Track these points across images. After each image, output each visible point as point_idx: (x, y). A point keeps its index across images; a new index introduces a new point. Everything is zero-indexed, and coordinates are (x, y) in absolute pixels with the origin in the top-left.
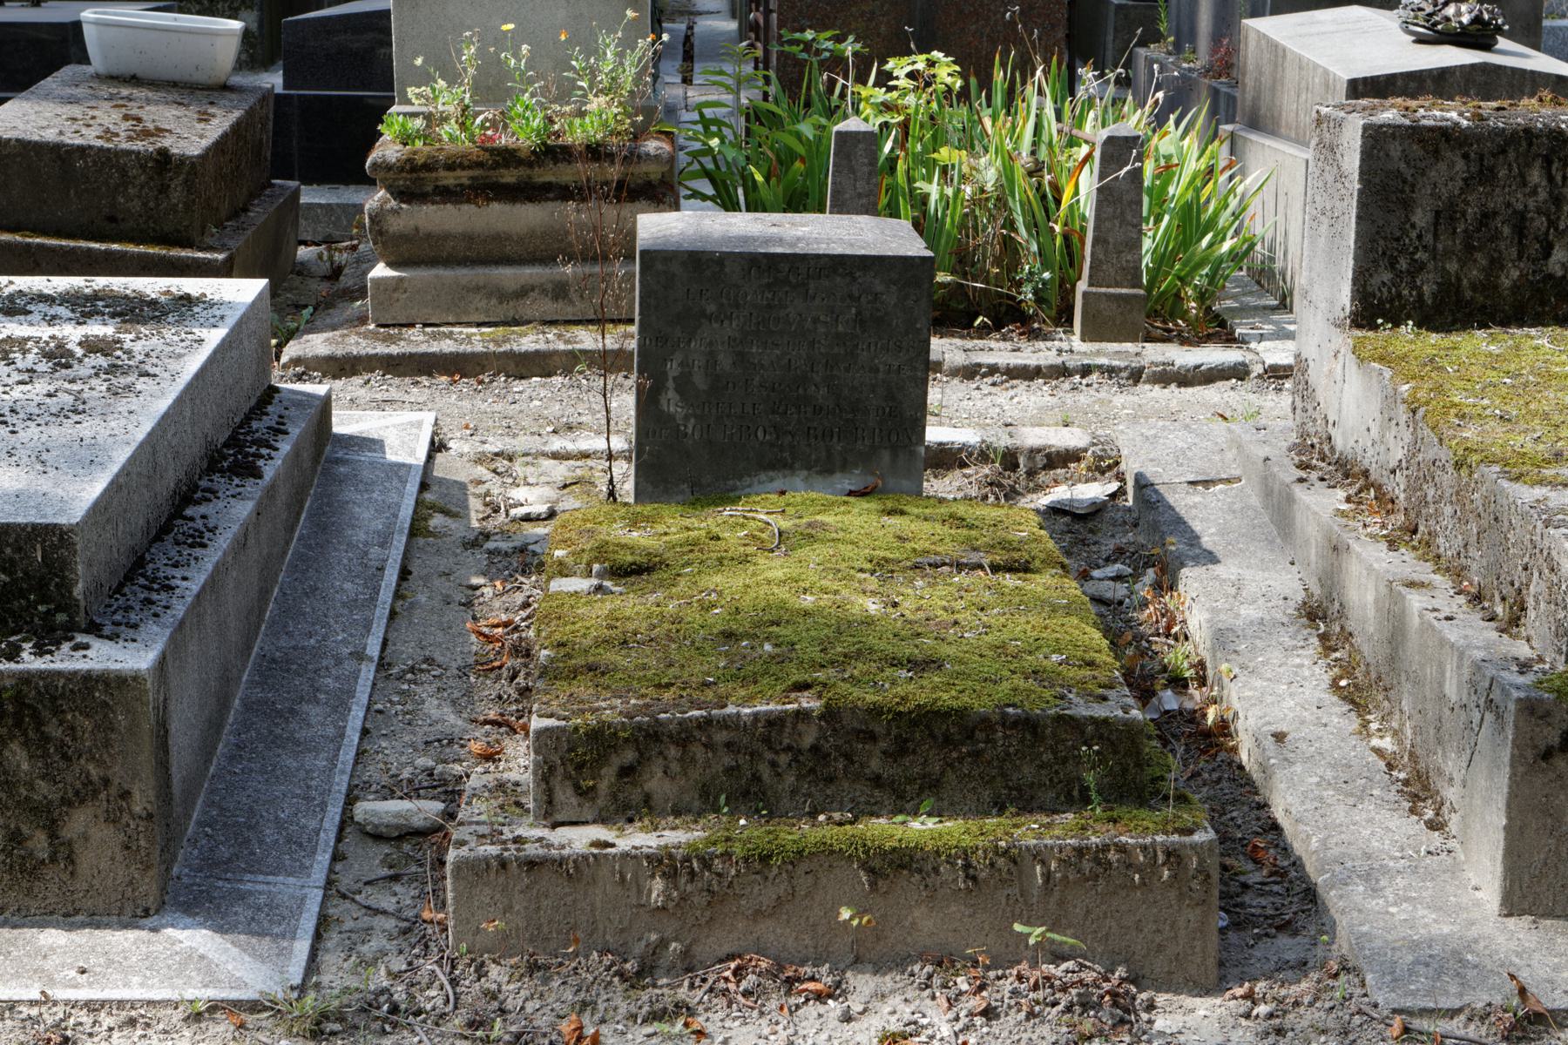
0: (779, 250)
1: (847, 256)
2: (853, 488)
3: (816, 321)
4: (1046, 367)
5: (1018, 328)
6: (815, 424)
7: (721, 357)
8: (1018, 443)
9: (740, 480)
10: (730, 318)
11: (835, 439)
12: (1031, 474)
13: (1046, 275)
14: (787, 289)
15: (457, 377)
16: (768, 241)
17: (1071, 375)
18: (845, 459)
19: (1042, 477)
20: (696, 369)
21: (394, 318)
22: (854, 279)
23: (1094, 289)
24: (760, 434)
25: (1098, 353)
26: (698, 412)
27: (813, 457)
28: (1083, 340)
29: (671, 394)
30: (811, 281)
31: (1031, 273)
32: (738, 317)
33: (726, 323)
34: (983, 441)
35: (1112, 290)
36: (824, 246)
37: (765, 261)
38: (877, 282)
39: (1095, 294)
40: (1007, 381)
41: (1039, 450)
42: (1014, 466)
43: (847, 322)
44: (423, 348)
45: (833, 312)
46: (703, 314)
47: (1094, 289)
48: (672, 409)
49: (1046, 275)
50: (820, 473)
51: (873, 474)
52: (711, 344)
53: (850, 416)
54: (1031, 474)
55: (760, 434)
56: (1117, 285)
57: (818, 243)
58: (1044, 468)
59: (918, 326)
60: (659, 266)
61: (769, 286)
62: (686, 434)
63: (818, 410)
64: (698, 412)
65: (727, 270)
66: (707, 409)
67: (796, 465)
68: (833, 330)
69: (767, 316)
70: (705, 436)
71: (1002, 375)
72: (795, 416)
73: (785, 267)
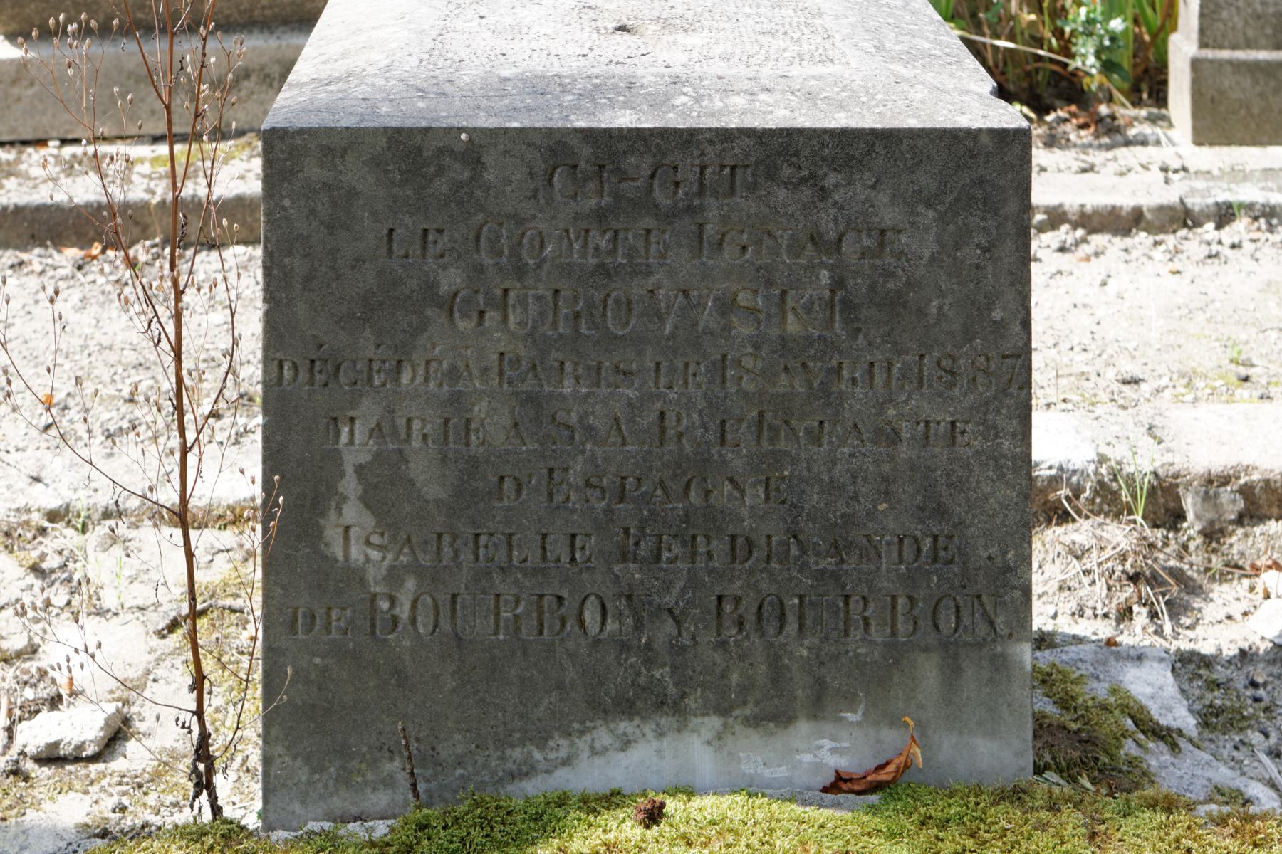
0: (624, 119)
1: (801, 131)
2: (843, 763)
3: (726, 306)
4: (1150, 210)
5: (1074, 115)
6: (736, 588)
7: (480, 409)
8: (1179, 462)
9: (542, 745)
10: (502, 304)
11: (791, 628)
12: (1213, 535)
13: (1117, 24)
14: (648, 222)
15: (96, 249)
16: (596, 91)
17: (1198, 224)
18: (820, 682)
19: (1238, 543)
20: (416, 444)
21: (13, 131)
22: (823, 193)
23: (1209, 54)
24: (591, 616)
25: (1237, 175)
26: (426, 560)
27: (735, 678)
28: (1200, 138)
29: (353, 512)
30: (709, 200)
31: (1090, 22)
32: (523, 301)
33: (492, 316)
34: (1102, 459)
35: (1240, 55)
36: (739, 101)
37: (587, 151)
38: (883, 198)
39: (1212, 62)
40: (1084, 240)
41: (1225, 480)
42: (1174, 518)
43: (809, 309)
44: (41, 196)
45: (769, 283)
46: (430, 292)
47: (1209, 54)
48: (356, 553)
49: (1117, 24)
50: (755, 722)
51: (895, 721)
52: (453, 374)
53: (828, 563)
54: (1213, 535)
55: (591, 616)
56: (1249, 44)
57: (726, 92)
58: (1240, 521)
59: (997, 314)
60: (313, 172)
61: (601, 215)
62: (395, 621)
63: (741, 547)
64: (426, 560)
65: (489, 176)
66: (447, 551)
67: (692, 702)
68: (774, 332)
69: (598, 297)
70: (445, 625)
71: (1075, 226)
72: (683, 565)
73: (640, 165)
